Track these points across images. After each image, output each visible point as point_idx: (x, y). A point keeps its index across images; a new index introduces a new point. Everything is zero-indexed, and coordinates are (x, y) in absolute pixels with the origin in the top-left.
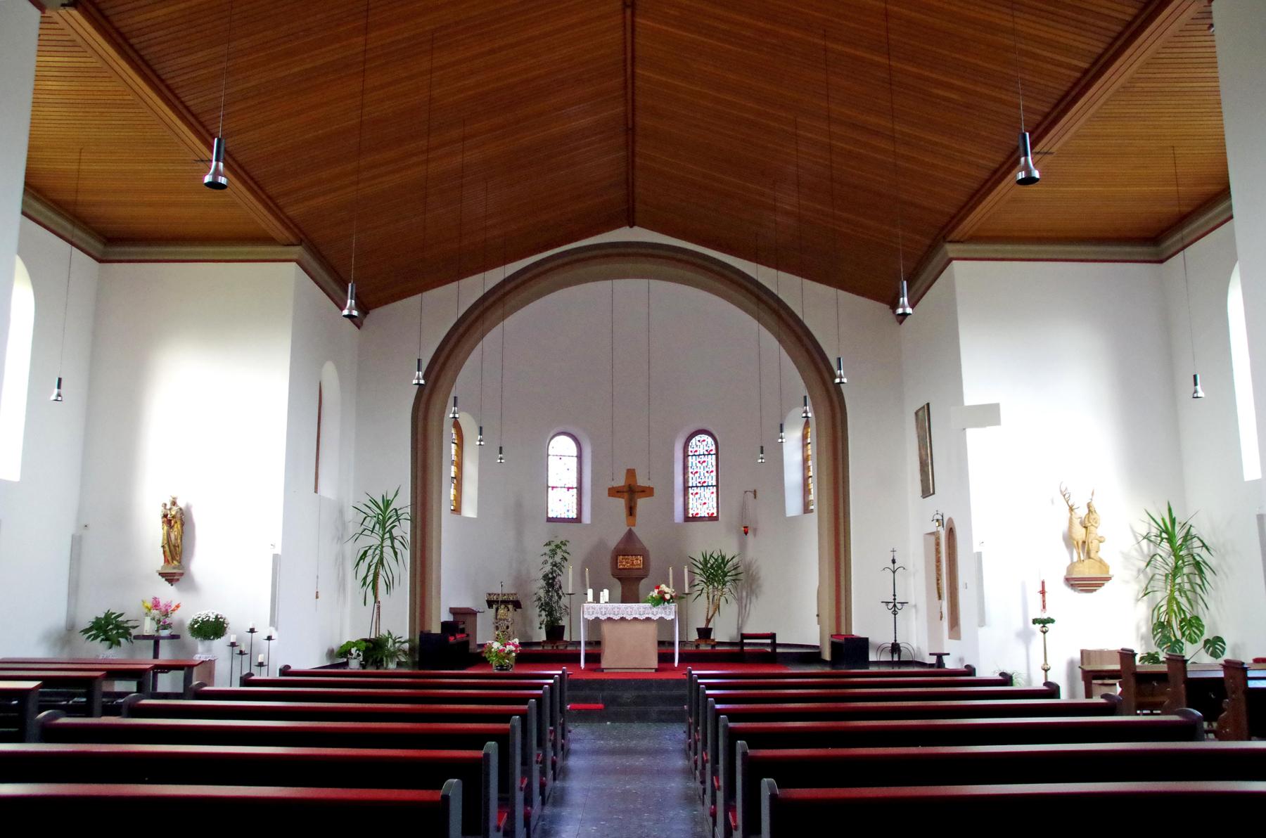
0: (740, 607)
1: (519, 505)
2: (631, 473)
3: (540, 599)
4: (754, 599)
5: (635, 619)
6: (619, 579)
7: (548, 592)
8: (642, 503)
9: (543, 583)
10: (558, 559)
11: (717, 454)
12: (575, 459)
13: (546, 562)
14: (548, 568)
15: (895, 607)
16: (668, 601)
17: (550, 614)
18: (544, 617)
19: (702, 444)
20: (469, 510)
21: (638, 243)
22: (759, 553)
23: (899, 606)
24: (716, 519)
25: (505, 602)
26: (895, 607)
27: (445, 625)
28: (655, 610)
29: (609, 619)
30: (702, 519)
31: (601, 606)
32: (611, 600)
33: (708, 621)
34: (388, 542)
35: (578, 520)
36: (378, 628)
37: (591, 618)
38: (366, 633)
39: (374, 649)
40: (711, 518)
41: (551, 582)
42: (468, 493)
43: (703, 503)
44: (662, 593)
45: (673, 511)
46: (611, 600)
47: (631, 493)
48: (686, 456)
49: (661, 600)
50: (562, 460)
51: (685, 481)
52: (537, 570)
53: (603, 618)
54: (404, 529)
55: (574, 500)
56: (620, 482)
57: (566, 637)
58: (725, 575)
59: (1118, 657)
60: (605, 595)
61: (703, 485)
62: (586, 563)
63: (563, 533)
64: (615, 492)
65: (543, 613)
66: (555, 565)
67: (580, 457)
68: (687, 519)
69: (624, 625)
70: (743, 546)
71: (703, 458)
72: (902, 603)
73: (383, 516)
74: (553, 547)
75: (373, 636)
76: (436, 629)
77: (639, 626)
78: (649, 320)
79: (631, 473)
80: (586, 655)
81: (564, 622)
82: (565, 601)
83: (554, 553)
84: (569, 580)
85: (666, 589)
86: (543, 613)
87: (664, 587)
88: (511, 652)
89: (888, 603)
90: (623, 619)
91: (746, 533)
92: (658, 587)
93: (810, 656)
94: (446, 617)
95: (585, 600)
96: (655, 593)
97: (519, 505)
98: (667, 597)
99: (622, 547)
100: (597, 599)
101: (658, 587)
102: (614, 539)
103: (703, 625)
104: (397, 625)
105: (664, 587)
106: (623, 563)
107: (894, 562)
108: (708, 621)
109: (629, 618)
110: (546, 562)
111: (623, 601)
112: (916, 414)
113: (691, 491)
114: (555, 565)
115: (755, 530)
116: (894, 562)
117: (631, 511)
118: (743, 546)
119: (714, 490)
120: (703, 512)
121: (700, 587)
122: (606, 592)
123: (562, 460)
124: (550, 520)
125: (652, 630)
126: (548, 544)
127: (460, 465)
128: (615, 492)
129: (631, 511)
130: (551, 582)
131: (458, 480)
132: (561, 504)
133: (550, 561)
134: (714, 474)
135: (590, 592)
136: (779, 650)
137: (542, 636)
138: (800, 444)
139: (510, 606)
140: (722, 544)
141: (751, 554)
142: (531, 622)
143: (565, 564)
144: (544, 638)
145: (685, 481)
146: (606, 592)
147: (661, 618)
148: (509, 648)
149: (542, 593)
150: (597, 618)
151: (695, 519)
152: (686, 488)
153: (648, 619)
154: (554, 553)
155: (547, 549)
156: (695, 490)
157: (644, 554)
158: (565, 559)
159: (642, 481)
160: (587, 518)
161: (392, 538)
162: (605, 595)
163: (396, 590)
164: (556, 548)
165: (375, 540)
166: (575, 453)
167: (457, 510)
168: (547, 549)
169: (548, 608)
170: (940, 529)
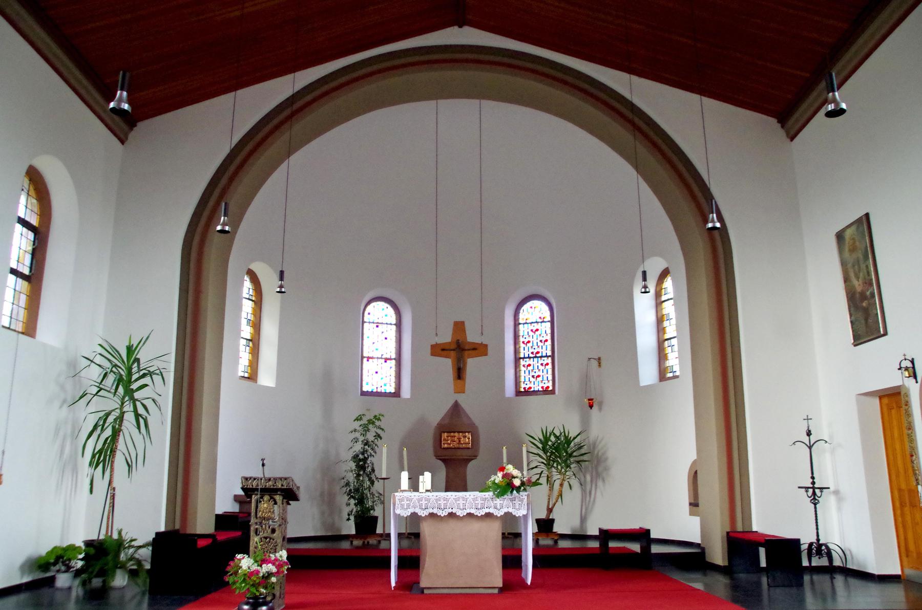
0: (584, 491)
1: (327, 376)
2: (459, 327)
3: (348, 484)
4: (600, 483)
5: (470, 515)
6: (444, 461)
7: (358, 475)
8: (472, 364)
9: (353, 465)
10: (370, 436)
11: (552, 322)
12: (394, 327)
13: (356, 440)
14: (358, 447)
15: (814, 493)
16: (518, 489)
17: (361, 501)
18: (352, 506)
19: (536, 311)
20: (267, 378)
21: (463, 46)
22: (607, 430)
23: (817, 491)
24: (553, 392)
25: (265, 491)
26: (814, 493)
27: (222, 521)
28: (498, 502)
29: (432, 515)
30: (535, 393)
31: (413, 497)
32: (434, 488)
33: (550, 510)
34: (128, 407)
35: (397, 394)
36: (110, 526)
37: (406, 513)
38: (80, 533)
39: (101, 554)
40: (546, 391)
41: (362, 463)
42: (256, 348)
43: (536, 375)
44: (509, 477)
45: (504, 386)
46: (434, 488)
47: (459, 351)
48: (516, 324)
49: (508, 487)
50: (379, 330)
51: (516, 351)
52: (347, 449)
53: (423, 513)
54: (160, 395)
55: (393, 372)
56: (446, 337)
57: (379, 530)
58: (571, 455)
59: (468, 487)
60: (426, 480)
61: (536, 356)
62: (409, 441)
63: (378, 407)
64: (439, 350)
65: (353, 502)
66: (366, 443)
67: (399, 325)
68: (518, 393)
69: (452, 523)
70: (585, 422)
71: (536, 326)
72: (821, 489)
73: (126, 374)
74: (364, 421)
75: (102, 537)
76: (203, 525)
77: (476, 526)
78: (478, 161)
79: (459, 327)
80: (401, 559)
81: (377, 512)
82: (378, 486)
83: (366, 429)
84: (382, 462)
85: (515, 472)
86: (353, 502)
87: (510, 469)
88: (270, 574)
89: (807, 488)
90: (452, 515)
91: (591, 406)
92: (502, 469)
93: (692, 559)
94: (225, 504)
95: (397, 487)
96: (498, 478)
97: (327, 376)
98: (517, 482)
99: (447, 421)
100: (414, 486)
101: (502, 469)
102: (437, 414)
103: (543, 516)
104: (142, 519)
105: (510, 469)
106: (448, 441)
107: (809, 433)
108: (550, 510)
109: (460, 513)
110: (356, 440)
111: (447, 489)
112: (840, 236)
113: (522, 362)
114: (366, 443)
115: (601, 404)
116: (809, 433)
117: (460, 373)
118: (585, 422)
119: (549, 360)
120: (537, 387)
121: (538, 471)
122: (427, 476)
123: (379, 330)
124: (364, 393)
125: (494, 531)
126: (358, 419)
127: (256, 325)
128: (439, 350)
129: (460, 373)
130: (362, 463)
131: (255, 343)
132: (378, 376)
133: (361, 438)
134: (549, 343)
135: (405, 476)
136: (655, 549)
137: (350, 528)
138: (653, 303)
139: (278, 498)
140: (561, 419)
141: (595, 432)
142: (340, 511)
143: (379, 442)
144: (353, 531)
145: (516, 351)
146: (427, 476)
147: (508, 514)
148: (269, 568)
149: (351, 477)
150: (414, 515)
151: (527, 392)
152: (517, 360)
153: (489, 515)
154: (366, 429)
155: (357, 425)
156: (528, 362)
157: (473, 430)
158: (378, 436)
159: (472, 337)
160: (406, 393)
161: (134, 401)
162: (426, 480)
163: (140, 472)
164: (369, 423)
165: (110, 403)
166: (394, 322)
167: (252, 377)
168: (357, 425)
169: (359, 496)
170: (910, 383)
